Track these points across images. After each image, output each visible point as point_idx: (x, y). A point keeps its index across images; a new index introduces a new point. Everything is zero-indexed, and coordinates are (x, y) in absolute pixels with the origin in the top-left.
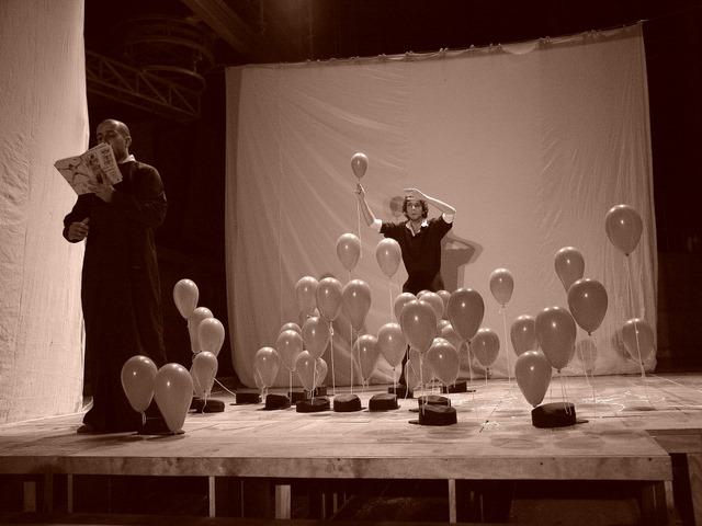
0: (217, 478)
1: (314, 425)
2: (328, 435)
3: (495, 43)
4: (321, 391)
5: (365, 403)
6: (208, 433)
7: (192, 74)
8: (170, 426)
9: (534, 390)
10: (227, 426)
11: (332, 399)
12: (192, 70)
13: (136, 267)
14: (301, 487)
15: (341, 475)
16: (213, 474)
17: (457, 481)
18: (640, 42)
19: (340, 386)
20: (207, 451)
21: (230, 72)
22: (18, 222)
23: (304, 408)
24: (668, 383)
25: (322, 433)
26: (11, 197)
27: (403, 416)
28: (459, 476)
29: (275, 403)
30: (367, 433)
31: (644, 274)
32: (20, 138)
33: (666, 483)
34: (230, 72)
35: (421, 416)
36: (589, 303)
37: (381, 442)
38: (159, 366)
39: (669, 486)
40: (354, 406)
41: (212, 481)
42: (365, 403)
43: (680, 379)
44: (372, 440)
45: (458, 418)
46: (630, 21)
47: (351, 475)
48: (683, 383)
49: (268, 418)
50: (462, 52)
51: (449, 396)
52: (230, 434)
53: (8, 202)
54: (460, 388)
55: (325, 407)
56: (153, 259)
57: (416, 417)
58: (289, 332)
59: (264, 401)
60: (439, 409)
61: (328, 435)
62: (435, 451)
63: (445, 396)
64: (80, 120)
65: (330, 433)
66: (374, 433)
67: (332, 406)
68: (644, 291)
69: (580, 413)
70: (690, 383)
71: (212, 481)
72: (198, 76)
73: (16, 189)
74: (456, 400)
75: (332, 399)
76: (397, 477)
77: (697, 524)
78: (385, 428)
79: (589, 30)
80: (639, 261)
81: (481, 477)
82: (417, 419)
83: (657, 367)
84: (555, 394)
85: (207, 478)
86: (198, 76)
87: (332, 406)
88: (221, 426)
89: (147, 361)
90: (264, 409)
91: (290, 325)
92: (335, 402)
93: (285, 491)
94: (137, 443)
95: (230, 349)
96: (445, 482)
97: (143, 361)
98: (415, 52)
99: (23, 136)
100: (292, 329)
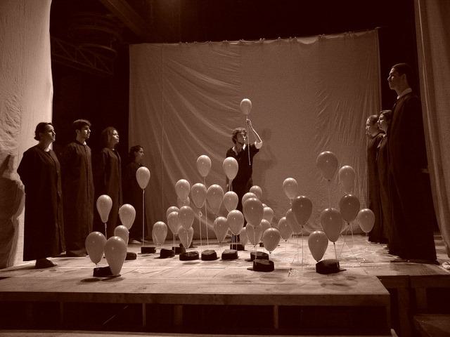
0: (147, 305)
1: (194, 270)
2: (205, 278)
3: (293, 37)
5: (219, 254)
7: (110, 49)
9: (317, 247)
12: (109, 47)
13: (61, 154)
14: (186, 307)
15: (217, 303)
16: (277, 304)
20: (139, 289)
21: (134, 49)
22: (14, 148)
23: (185, 257)
26: (10, 133)
27: (241, 267)
28: (280, 304)
30: (225, 277)
32: (16, 98)
34: (134, 49)
35: (254, 265)
36: (350, 206)
37: (236, 283)
39: (388, 308)
40: (210, 257)
42: (219, 254)
44: (231, 282)
46: (371, 28)
47: (222, 303)
49: (165, 264)
51: (233, 251)
52: (147, 276)
53: (9, 136)
56: (86, 163)
57: (251, 265)
58: (174, 213)
60: (263, 262)
62: (267, 290)
63: (233, 251)
65: (204, 276)
67: (200, 256)
68: (382, 214)
69: (342, 265)
72: (113, 50)
73: (14, 128)
74: (273, 255)
78: (235, 273)
79: (348, 31)
81: (293, 304)
82: (252, 267)
84: (329, 255)
85: (141, 304)
86: (113, 50)
87: (200, 256)
89: (100, 234)
90: (159, 258)
91: (173, 208)
92: (202, 255)
93: (181, 307)
94: (97, 283)
96: (273, 306)
99: (16, 96)
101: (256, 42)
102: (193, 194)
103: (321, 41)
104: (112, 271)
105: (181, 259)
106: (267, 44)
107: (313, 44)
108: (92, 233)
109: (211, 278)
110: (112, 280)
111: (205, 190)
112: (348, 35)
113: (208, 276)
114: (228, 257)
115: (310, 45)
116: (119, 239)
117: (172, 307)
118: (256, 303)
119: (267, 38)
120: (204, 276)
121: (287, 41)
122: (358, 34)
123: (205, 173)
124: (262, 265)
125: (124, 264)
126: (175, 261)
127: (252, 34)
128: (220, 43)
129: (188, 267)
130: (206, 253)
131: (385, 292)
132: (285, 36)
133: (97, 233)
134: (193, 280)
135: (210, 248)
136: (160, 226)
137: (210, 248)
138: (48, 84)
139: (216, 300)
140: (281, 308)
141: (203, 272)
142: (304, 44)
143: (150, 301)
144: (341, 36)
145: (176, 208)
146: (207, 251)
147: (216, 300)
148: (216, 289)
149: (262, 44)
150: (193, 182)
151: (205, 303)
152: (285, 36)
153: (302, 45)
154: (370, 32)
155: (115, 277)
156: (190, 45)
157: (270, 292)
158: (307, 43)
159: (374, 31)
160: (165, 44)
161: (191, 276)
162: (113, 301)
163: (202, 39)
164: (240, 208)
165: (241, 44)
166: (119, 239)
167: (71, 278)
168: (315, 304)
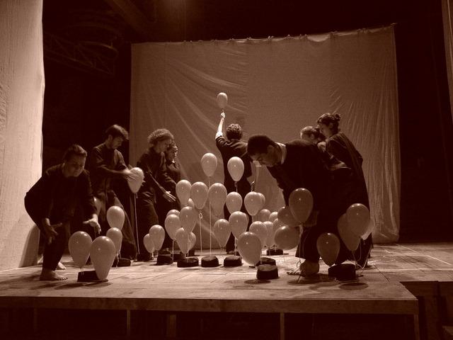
2: (201, 284)
3: (303, 34)
4: (192, 253)
5: (221, 261)
6: (122, 281)
7: (109, 47)
8: (99, 278)
10: (135, 277)
11: (200, 259)
14: (179, 314)
16: (283, 311)
17: (286, 314)
18: (392, 36)
19: (206, 249)
21: (135, 48)
23: (183, 264)
24: (407, 250)
25: (196, 282)
28: (286, 311)
29: (163, 261)
31: (393, 182)
33: (415, 316)
34: (135, 48)
37: (236, 288)
38: (93, 239)
39: (416, 317)
40: (212, 264)
41: (128, 312)
42: (221, 261)
43: (414, 247)
44: (230, 287)
45: (256, 273)
47: (219, 310)
48: (416, 250)
49: (160, 271)
50: (281, 39)
51: (272, 257)
52: (137, 281)
54: (279, 253)
55: (196, 264)
59: (156, 259)
61: (201, 284)
62: (272, 295)
63: (272, 257)
64: (39, 76)
66: (231, 282)
67: (200, 263)
70: (421, 250)
71: (128, 312)
75: (200, 259)
76: (248, 311)
77: (452, 334)
79: (361, 28)
80: (390, 174)
83: (399, 240)
85: (125, 311)
87: (200, 263)
88: (130, 276)
90: (156, 265)
91: (174, 211)
92: (202, 261)
93: (173, 317)
94: (80, 288)
95: (344, 245)
96: (278, 315)
97: (105, 240)
98: (252, 38)
100: (175, 214)
101: (265, 40)
102: (194, 192)
103: (333, 38)
104: (98, 275)
105: (179, 266)
106: (275, 42)
107: (324, 41)
108: (76, 233)
109: (208, 283)
110: (100, 284)
111: (206, 189)
112: (362, 31)
113: (205, 282)
114: (230, 264)
115: (322, 43)
116: (108, 240)
117: (166, 314)
118: (258, 310)
119: (276, 36)
120: (200, 282)
121: (297, 38)
122: (372, 31)
123: (209, 173)
124: (267, 274)
125: (110, 271)
126: (173, 268)
127: (260, 31)
128: (226, 42)
129: (185, 273)
130: (207, 259)
131: (412, 297)
132: (295, 34)
133: (82, 233)
134: (188, 286)
135: (210, 255)
136: (156, 229)
137: (210, 255)
138: (39, 76)
139: (212, 306)
140: (287, 315)
141: (201, 277)
142: (316, 43)
143: (135, 307)
144: (354, 33)
145: (177, 211)
146: (208, 256)
147: (212, 306)
148: (212, 294)
149: (270, 42)
150: (192, 182)
151: (199, 309)
152: (295, 33)
153: (313, 42)
154: (385, 29)
155: (101, 282)
156: (194, 44)
157: (275, 298)
158: (318, 41)
159: (389, 27)
160: (168, 43)
161: (187, 281)
162: (93, 307)
163: (196, 39)
164: (243, 210)
165: (249, 43)
166: (108, 240)
167: (242, 291)
168: (329, 312)
